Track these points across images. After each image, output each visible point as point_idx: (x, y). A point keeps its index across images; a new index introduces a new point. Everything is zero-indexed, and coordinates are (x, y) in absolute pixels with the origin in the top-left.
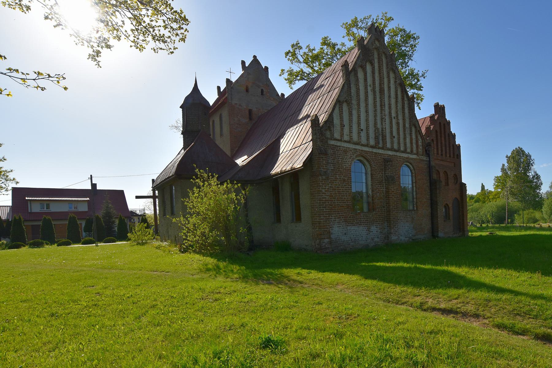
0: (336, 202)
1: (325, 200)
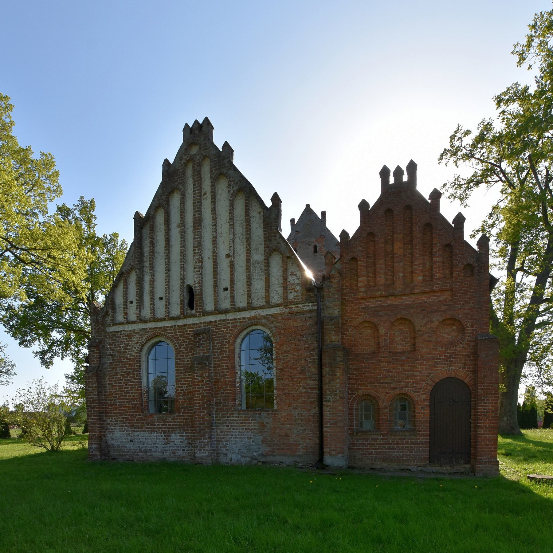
0: (117, 401)
1: (93, 401)
